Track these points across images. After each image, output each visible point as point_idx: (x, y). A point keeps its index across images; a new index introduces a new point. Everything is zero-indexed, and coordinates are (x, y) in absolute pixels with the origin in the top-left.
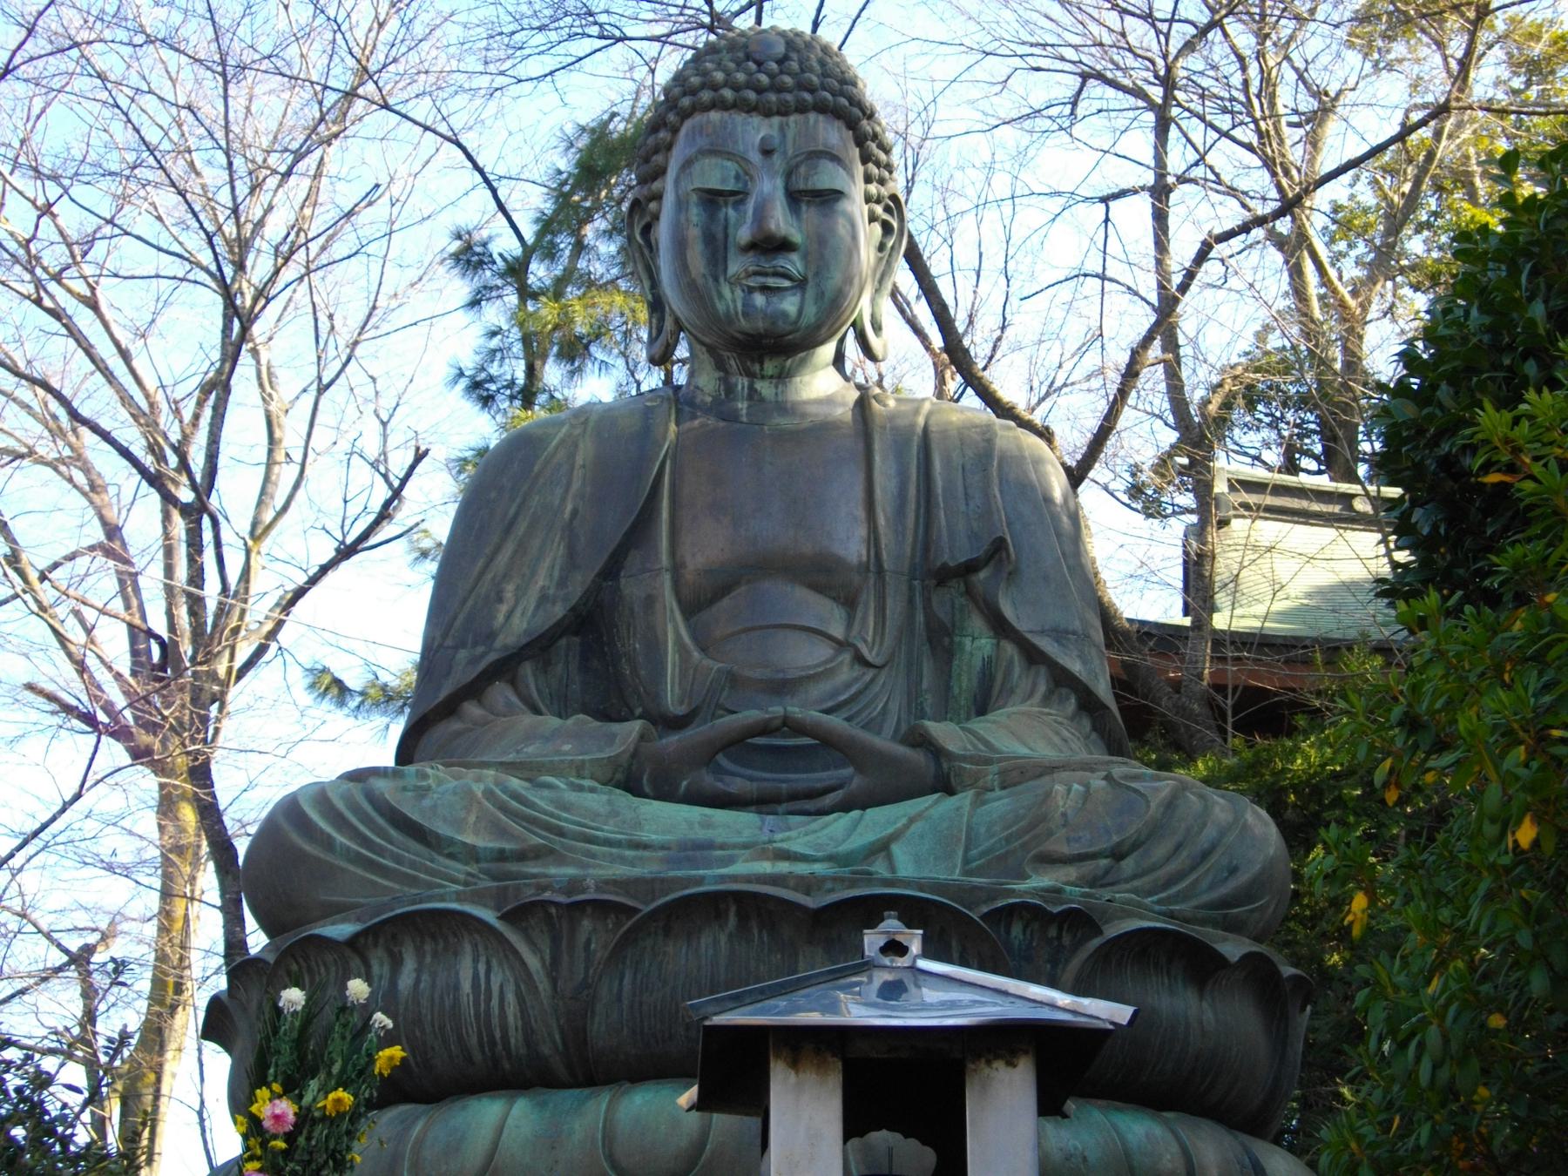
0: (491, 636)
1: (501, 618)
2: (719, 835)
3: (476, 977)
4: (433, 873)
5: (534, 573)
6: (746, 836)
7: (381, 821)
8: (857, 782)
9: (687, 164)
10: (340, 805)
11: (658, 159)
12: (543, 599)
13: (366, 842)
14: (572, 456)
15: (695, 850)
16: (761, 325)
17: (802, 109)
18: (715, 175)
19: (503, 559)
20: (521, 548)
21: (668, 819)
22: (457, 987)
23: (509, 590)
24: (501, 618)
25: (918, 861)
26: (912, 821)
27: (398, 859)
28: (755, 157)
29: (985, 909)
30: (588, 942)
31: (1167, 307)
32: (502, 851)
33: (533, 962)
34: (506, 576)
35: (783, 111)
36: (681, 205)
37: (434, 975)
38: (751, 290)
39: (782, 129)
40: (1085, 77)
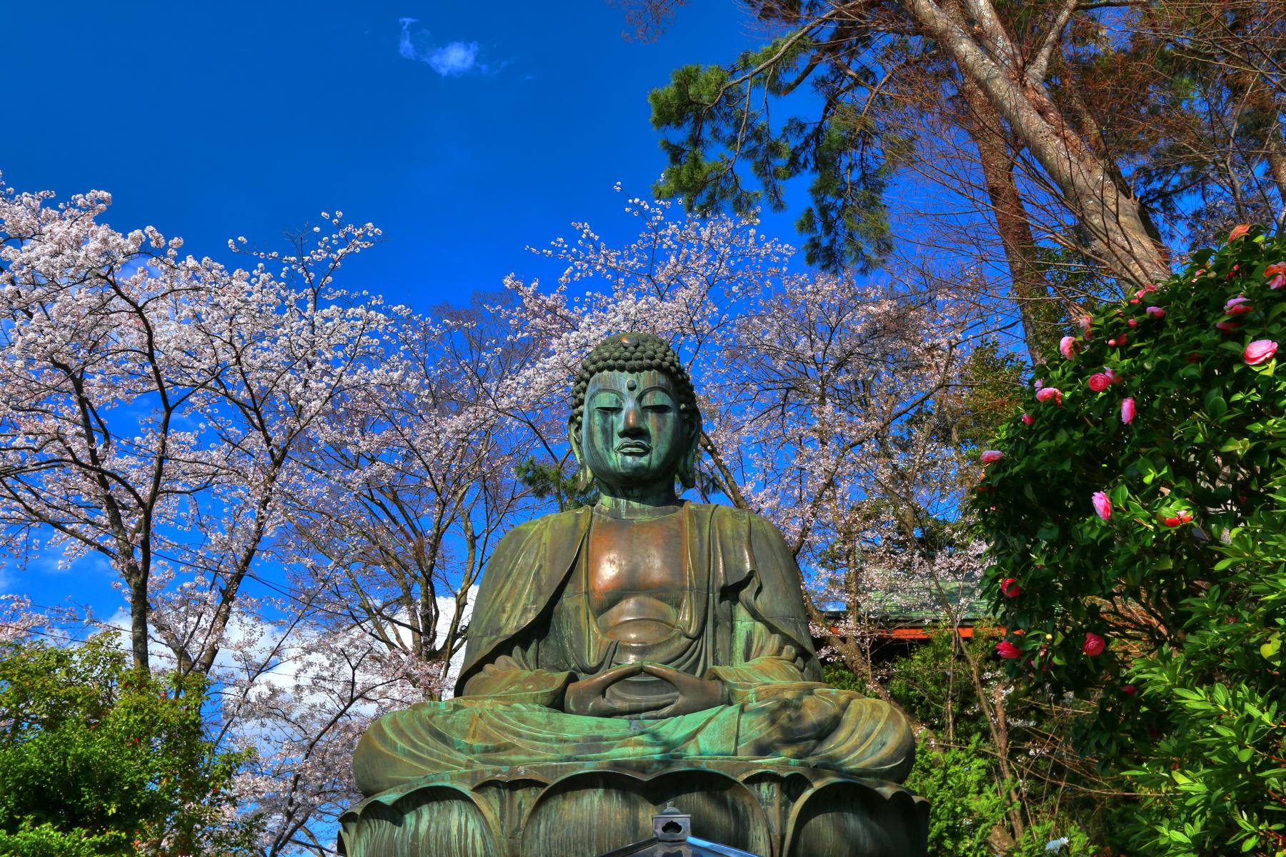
0: (499, 630)
1: (504, 620)
2: (605, 733)
3: (460, 824)
4: (448, 761)
5: (520, 597)
6: (621, 732)
7: (423, 732)
8: (681, 700)
9: (592, 397)
10: (402, 724)
11: (581, 395)
12: (525, 611)
13: (414, 745)
15: (595, 743)
18: (606, 400)
19: (505, 591)
20: (514, 584)
21: (577, 725)
22: (449, 832)
23: (509, 605)
24: (504, 620)
25: (712, 744)
26: (710, 720)
27: (430, 754)
28: (625, 390)
29: (745, 776)
30: (520, 804)
32: (486, 747)
33: (490, 816)
34: (507, 600)
35: (641, 369)
36: (591, 416)
37: (437, 823)
38: (625, 454)
40: (788, 390)
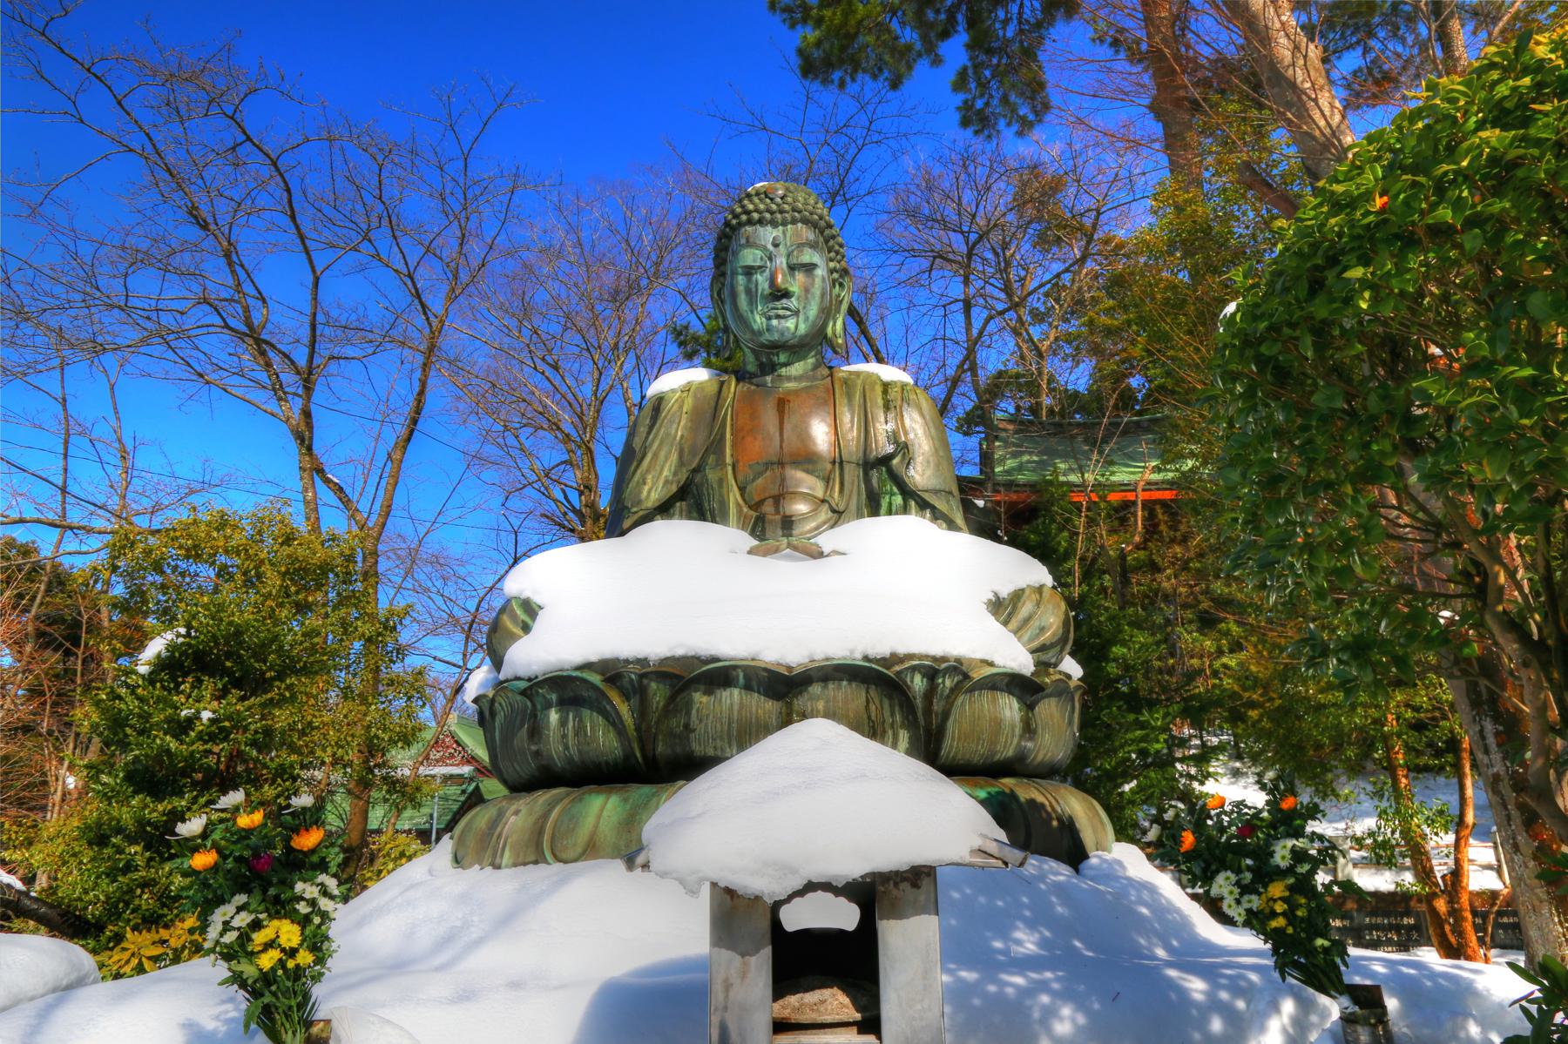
12: (666, 482)
14: (681, 407)
16: (776, 337)
17: (794, 222)
23: (649, 481)
31: (971, 353)
34: (648, 471)
35: (784, 224)
39: (784, 233)
